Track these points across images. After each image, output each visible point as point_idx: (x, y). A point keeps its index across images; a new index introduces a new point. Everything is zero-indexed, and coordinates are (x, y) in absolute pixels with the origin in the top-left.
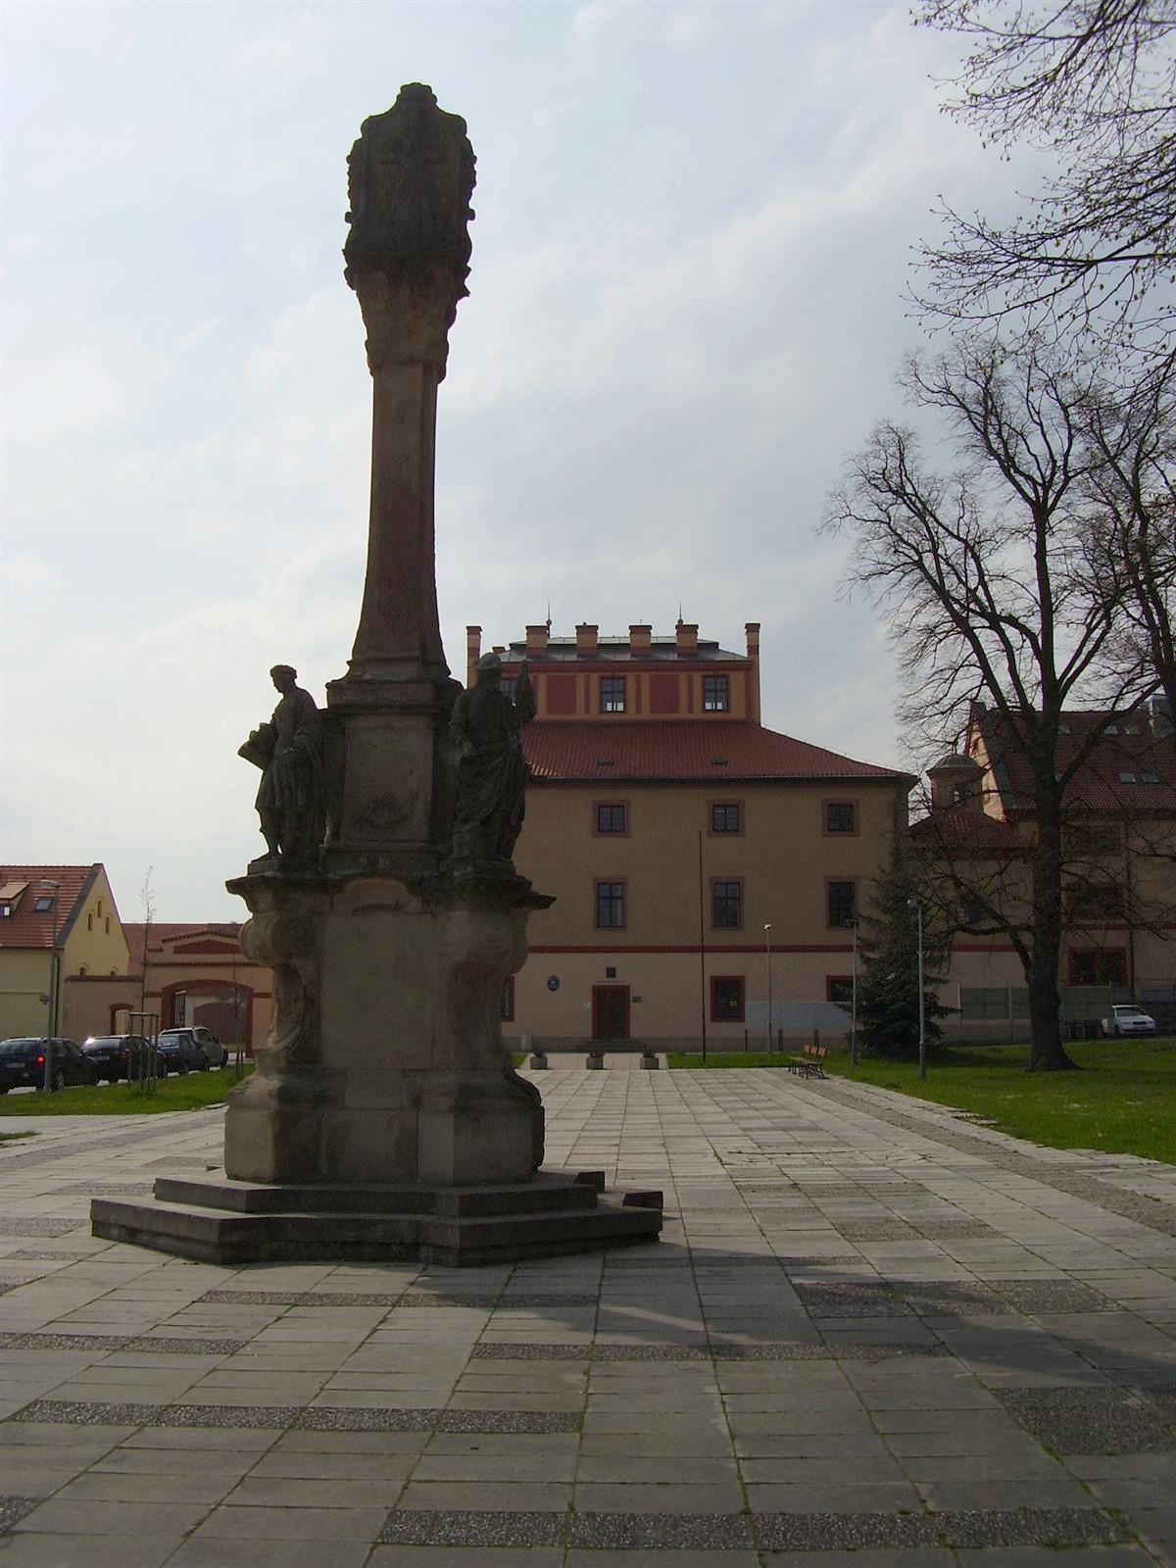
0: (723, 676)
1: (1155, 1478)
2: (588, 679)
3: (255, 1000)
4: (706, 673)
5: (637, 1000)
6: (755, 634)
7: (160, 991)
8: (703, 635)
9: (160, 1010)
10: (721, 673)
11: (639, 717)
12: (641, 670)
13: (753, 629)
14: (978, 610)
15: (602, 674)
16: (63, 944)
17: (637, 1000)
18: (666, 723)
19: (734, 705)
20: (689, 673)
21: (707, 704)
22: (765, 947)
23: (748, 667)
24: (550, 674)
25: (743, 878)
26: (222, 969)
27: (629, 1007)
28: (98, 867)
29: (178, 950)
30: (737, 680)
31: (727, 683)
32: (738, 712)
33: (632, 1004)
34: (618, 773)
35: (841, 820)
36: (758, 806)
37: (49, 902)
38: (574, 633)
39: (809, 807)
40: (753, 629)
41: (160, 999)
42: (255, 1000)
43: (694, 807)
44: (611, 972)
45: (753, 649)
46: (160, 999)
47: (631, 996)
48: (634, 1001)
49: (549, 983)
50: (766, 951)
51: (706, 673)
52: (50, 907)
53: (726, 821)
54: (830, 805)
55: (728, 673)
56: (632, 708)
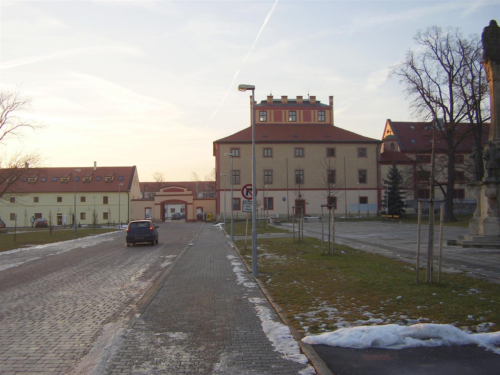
0: (323, 111)
1: (453, 316)
2: (285, 112)
3: (188, 205)
4: (319, 110)
5: (307, 204)
6: (332, 99)
7: (160, 203)
8: (317, 99)
9: (306, 206)
10: (294, 110)
11: (300, 123)
12: (301, 109)
13: (331, 98)
14: (422, 93)
15: (290, 110)
16: (130, 190)
17: (307, 204)
18: (277, 125)
19: (326, 119)
20: (285, 110)
21: (261, 118)
22: (266, 189)
23: (330, 108)
24: (304, 110)
25: (304, 169)
26: (188, 196)
27: (305, 205)
28: (134, 167)
29: (164, 191)
30: (327, 112)
31: (325, 113)
32: (327, 122)
33: (306, 204)
34: (274, 139)
35: (362, 153)
36: (340, 149)
37: (100, 178)
38: (281, 98)
39: (353, 149)
40: (331, 98)
41: (160, 206)
42: (188, 205)
43: (322, 149)
44: (300, 196)
45: (331, 103)
46: (160, 206)
47: (306, 202)
48: (307, 204)
49: (283, 199)
50: (224, 191)
51: (319, 110)
52: (57, 180)
53: (331, 153)
54: (328, 149)
55: (266, 110)
56: (268, 119)
